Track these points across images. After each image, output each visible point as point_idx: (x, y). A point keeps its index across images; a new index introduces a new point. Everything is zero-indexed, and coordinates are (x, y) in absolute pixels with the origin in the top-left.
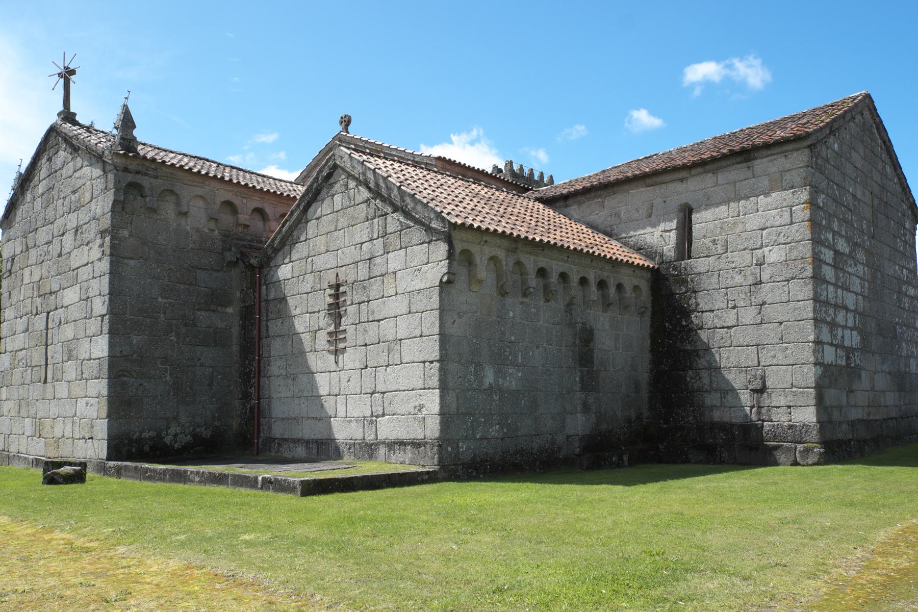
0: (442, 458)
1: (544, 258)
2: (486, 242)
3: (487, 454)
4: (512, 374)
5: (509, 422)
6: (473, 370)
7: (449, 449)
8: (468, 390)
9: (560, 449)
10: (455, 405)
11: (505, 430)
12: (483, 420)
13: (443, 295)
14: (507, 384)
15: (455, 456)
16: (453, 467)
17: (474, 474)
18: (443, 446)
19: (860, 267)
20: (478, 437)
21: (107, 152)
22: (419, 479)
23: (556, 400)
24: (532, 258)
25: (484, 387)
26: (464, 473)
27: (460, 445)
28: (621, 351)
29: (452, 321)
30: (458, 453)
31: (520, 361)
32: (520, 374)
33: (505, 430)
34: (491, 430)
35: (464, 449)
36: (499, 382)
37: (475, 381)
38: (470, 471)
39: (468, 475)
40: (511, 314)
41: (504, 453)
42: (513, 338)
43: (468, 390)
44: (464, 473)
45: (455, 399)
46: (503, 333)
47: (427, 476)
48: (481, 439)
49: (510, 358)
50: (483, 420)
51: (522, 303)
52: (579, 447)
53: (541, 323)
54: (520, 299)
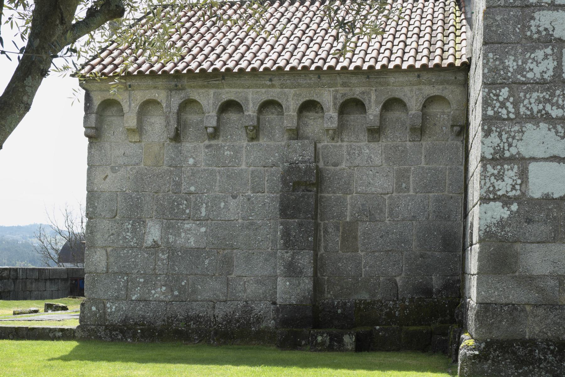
0: (84, 317)
1: (231, 87)
2: (130, 86)
3: (144, 317)
4: (190, 230)
5: (183, 283)
6: (130, 226)
7: (94, 308)
8: (123, 248)
9: (259, 320)
10: (104, 264)
11: (176, 293)
12: (142, 280)
13: (93, 150)
14: (180, 241)
15: (100, 316)
16: (93, 327)
17: (120, 337)
18: (86, 305)
19: (515, 64)
20: (134, 298)
21: (110, 15)
22: (51, 335)
23: (266, 260)
24: (212, 92)
25: (145, 245)
26: (107, 335)
27: (108, 305)
28: (411, 192)
29: (104, 176)
30: (105, 313)
31: (203, 214)
32: (203, 230)
33: (176, 293)
34: (153, 292)
35: (113, 310)
36: (168, 239)
37: (132, 239)
38: (114, 333)
39: (111, 337)
40: (191, 161)
41: (168, 318)
42: (192, 189)
43: (123, 248)
44: (107, 335)
45: (104, 258)
46: (178, 184)
47: (61, 333)
48: (139, 300)
49: (187, 211)
50: (142, 280)
51: (208, 147)
52: (274, 319)
53: (243, 167)
54: (207, 142)
